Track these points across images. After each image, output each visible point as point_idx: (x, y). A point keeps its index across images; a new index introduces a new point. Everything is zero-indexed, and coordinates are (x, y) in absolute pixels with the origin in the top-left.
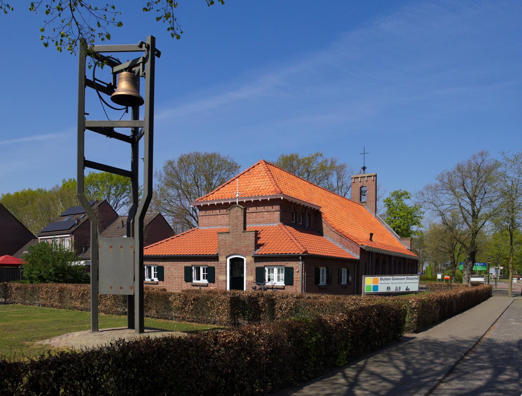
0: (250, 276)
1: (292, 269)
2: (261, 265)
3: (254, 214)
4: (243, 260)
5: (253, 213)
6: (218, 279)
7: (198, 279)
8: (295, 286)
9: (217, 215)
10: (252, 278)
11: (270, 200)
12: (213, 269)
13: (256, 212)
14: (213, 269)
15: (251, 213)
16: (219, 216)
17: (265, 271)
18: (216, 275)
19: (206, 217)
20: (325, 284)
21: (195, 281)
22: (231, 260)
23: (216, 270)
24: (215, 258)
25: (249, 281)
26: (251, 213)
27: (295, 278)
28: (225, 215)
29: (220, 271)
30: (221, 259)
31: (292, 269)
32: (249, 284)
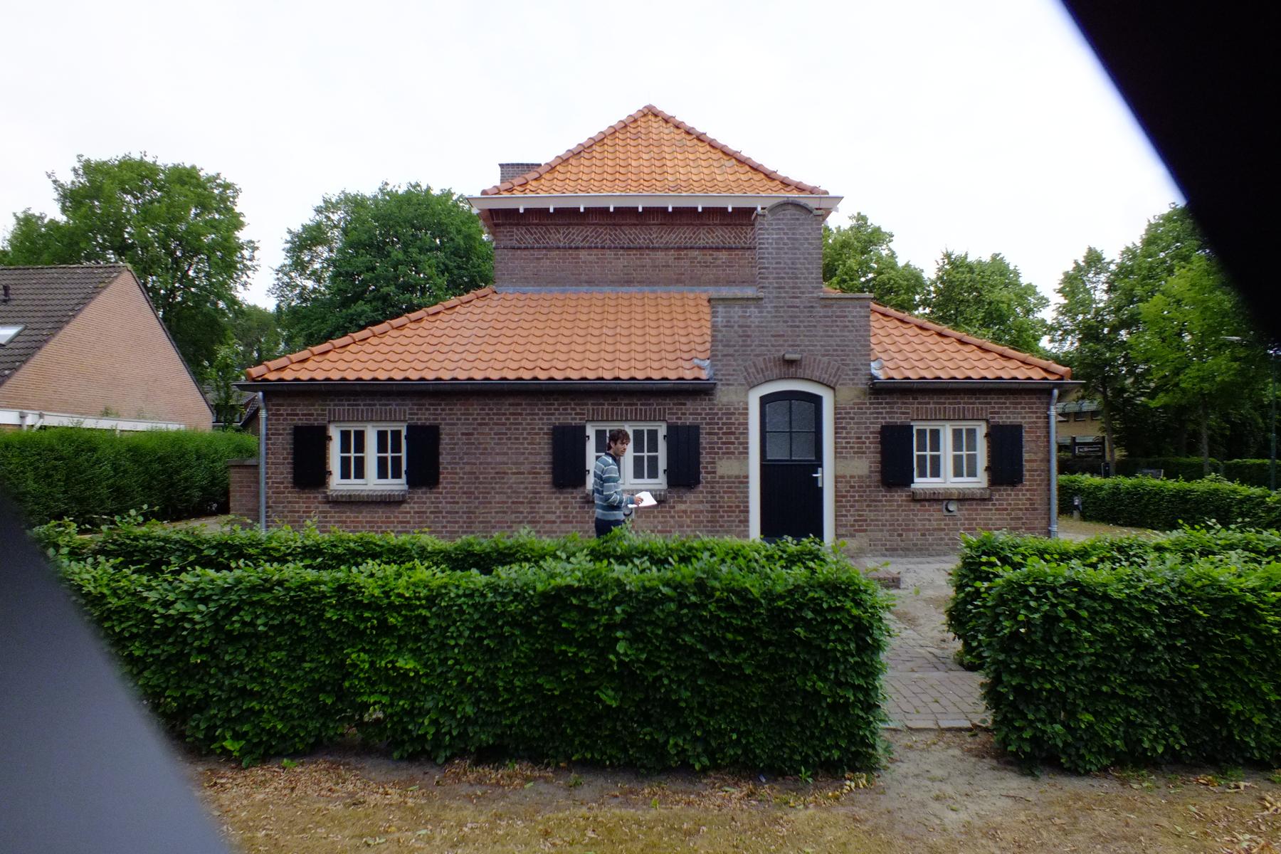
0: (852, 458)
1: (1018, 429)
2: (897, 414)
3: (723, 255)
4: (816, 400)
5: (717, 249)
6: (714, 473)
7: (354, 468)
8: (1027, 490)
9: (577, 248)
10: (863, 466)
11: (526, 210)
12: (694, 431)
13: (730, 249)
14: (694, 431)
15: (711, 248)
16: (583, 254)
17: (584, 438)
18: (705, 458)
19: (526, 252)
20: (984, 484)
21: (336, 483)
22: (765, 400)
23: (704, 440)
24: (699, 391)
25: (852, 477)
26: (711, 248)
27: (1027, 461)
28: (608, 252)
29: (724, 443)
30: (724, 396)
31: (1018, 429)
32: (852, 487)
